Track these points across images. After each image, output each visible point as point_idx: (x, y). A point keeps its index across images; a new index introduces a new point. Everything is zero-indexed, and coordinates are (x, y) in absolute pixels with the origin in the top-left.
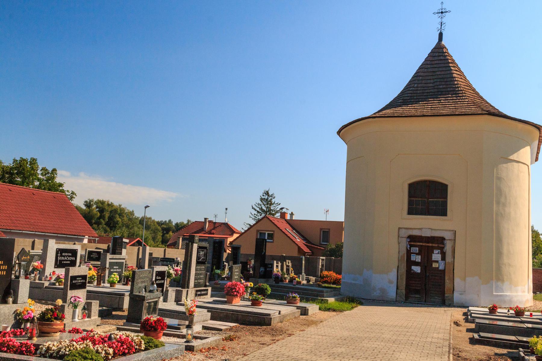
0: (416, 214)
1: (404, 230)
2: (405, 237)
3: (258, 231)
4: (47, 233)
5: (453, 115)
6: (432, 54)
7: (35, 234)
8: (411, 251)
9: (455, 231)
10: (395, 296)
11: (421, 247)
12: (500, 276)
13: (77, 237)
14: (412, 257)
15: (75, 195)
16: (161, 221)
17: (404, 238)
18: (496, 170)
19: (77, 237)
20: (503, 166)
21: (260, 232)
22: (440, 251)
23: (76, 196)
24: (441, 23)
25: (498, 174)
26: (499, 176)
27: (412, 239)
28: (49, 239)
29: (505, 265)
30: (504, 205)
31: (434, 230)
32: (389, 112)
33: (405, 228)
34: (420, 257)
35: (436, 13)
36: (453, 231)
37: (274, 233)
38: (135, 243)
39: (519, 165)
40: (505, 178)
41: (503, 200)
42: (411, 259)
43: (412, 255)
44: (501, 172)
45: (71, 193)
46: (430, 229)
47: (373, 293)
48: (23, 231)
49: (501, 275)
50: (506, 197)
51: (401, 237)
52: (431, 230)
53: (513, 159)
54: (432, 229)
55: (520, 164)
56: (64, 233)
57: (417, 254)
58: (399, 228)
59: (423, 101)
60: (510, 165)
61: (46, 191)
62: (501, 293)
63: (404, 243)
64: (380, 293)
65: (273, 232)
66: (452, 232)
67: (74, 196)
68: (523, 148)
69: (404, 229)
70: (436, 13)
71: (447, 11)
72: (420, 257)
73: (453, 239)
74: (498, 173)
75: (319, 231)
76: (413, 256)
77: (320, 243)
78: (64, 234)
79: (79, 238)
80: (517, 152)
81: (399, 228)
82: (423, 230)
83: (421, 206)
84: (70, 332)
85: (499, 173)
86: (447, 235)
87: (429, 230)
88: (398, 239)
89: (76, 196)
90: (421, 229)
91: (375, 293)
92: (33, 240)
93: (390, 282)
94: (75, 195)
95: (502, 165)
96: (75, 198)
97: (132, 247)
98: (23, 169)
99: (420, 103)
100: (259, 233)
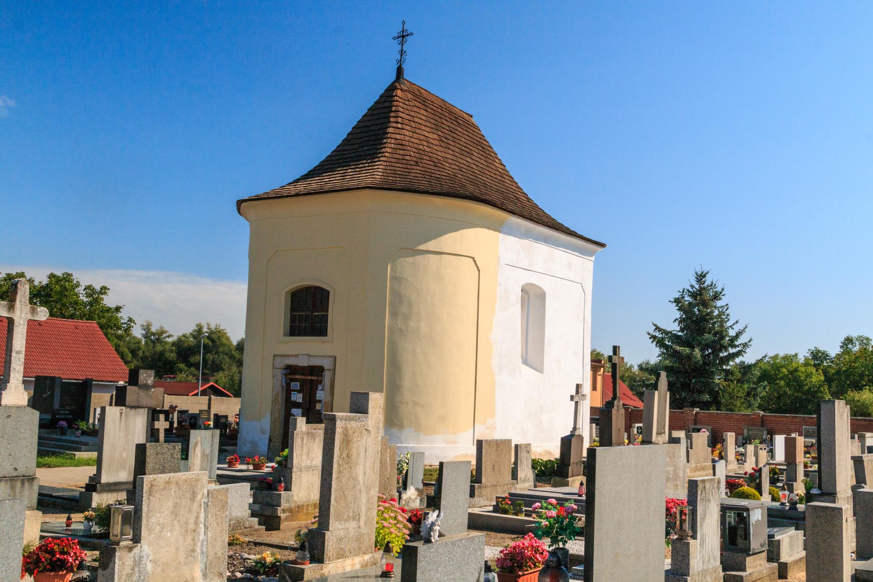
0: (299, 335)
1: (279, 359)
2: (280, 368)
4: (101, 381)
5: (322, 193)
8: (291, 388)
9: (336, 357)
10: (267, 451)
11: (303, 383)
12: (396, 420)
13: (97, 383)
14: (292, 395)
15: (134, 322)
16: (785, 358)
17: (279, 370)
18: (392, 268)
19: (97, 383)
20: (406, 260)
22: (299, 383)
23: (136, 324)
24: (402, 52)
25: (396, 272)
27: (291, 371)
28: (383, 394)
29: (407, 403)
30: (407, 317)
31: (313, 356)
33: (280, 355)
34: (301, 395)
35: (409, 35)
36: (333, 356)
38: (206, 388)
39: (442, 258)
40: (409, 279)
41: (404, 309)
42: (291, 398)
43: (292, 392)
44: (402, 270)
45: (128, 321)
46: (306, 355)
47: (243, 448)
49: (397, 419)
50: (410, 306)
51: (276, 368)
52: (307, 356)
53: (426, 249)
55: (444, 256)
56: (109, 379)
57: (299, 392)
58: (275, 356)
59: (328, 172)
60: (420, 258)
61: (59, 319)
62: (408, 444)
63: (279, 374)
64: (250, 448)
66: (332, 359)
67: (132, 324)
68: (462, 229)
69: (279, 357)
70: (409, 35)
71: (409, 33)
72: (301, 395)
73: (332, 368)
74: (396, 270)
76: (293, 394)
79: (100, 384)
80: (436, 238)
81: (275, 356)
83: (303, 323)
86: (326, 364)
87: (307, 356)
88: (273, 370)
89: (136, 324)
90: (297, 356)
91: (245, 448)
93: (263, 432)
94: (134, 322)
95: (403, 259)
96: (133, 327)
97: (195, 397)
98: (51, 290)
99: (324, 175)
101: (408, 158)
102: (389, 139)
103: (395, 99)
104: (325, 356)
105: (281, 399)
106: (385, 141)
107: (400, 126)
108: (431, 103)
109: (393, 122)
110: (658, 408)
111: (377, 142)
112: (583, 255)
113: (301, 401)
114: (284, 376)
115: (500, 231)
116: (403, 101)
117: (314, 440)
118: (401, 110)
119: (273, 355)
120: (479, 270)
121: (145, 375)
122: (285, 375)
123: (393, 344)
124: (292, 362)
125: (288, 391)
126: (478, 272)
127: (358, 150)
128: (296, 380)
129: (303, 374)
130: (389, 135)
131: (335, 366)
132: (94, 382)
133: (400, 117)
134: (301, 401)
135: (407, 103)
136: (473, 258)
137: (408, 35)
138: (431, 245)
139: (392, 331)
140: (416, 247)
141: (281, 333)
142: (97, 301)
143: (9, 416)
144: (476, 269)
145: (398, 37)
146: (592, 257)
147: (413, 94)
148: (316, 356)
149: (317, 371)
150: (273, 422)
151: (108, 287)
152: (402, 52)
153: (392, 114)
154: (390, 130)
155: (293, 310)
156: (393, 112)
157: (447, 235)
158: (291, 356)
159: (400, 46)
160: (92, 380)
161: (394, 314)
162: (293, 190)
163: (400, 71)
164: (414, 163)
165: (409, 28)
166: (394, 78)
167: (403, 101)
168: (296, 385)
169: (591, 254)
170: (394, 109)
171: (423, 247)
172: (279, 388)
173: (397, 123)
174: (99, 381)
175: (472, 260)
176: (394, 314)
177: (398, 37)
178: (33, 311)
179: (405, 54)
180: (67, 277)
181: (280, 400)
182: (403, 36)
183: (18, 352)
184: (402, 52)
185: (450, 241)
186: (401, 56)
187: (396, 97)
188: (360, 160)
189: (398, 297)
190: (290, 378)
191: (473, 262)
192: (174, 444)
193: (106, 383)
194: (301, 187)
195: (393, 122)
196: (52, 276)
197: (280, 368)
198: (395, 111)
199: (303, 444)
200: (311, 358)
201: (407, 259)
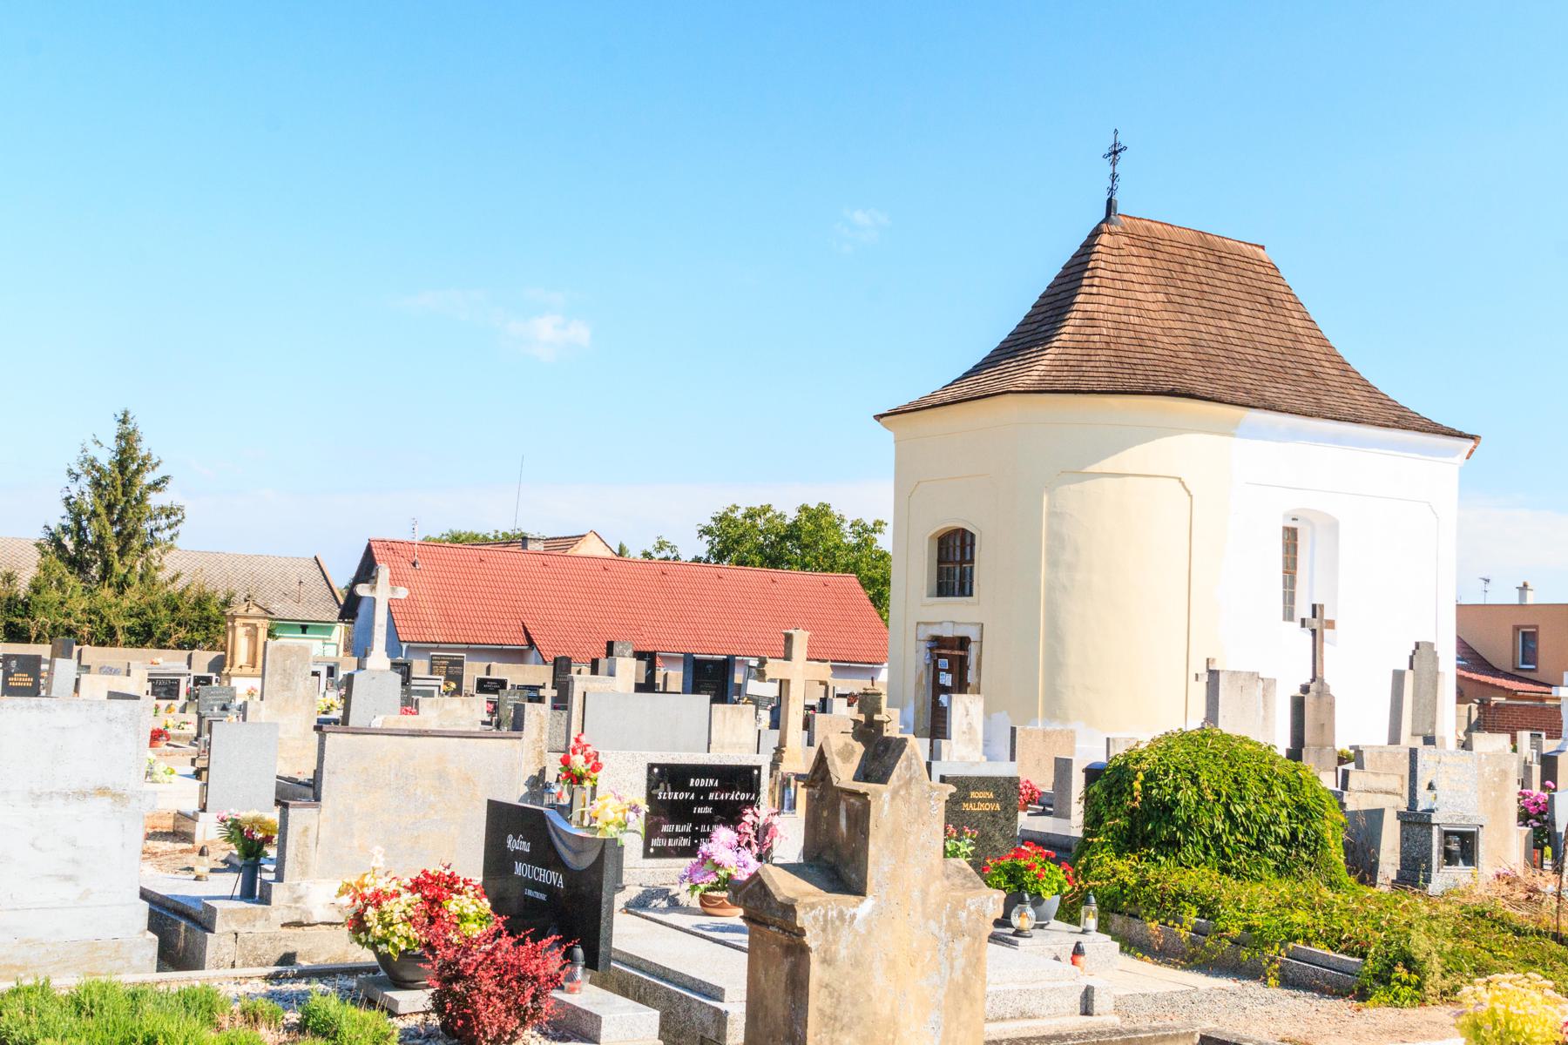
1: (922, 627)
3: (1518, 630)
4: (855, 662)
6: (1083, 250)
7: (502, 649)
9: (982, 625)
11: (951, 658)
19: (848, 665)
21: (1525, 630)
25: (1055, 506)
26: (1059, 511)
27: (938, 643)
32: (986, 381)
37: (1538, 631)
48: (744, 656)
54: (954, 622)
57: (948, 671)
58: (918, 623)
60: (1090, 485)
63: (923, 646)
65: (1534, 630)
73: (979, 639)
75: (1533, 623)
77: (1513, 665)
78: (845, 662)
79: (506, 649)
82: (944, 624)
84: (190, 668)
85: (1057, 505)
86: (972, 634)
92: (487, 664)
100: (1520, 634)
101: (1096, 338)
102: (1075, 313)
103: (1096, 250)
104: (971, 624)
105: (926, 681)
106: (1068, 316)
107: (1094, 290)
108: (1168, 243)
109: (1086, 286)
110: (1415, 703)
111: (1059, 318)
112: (1432, 456)
113: (950, 684)
114: (928, 651)
115: (1233, 435)
116: (1108, 251)
117: (742, 715)
118: (1102, 265)
119: (1537, 624)
120: (1191, 496)
121: (621, 647)
122: (931, 649)
123: (1051, 603)
124: (937, 631)
125: (937, 672)
126: (1189, 498)
127: (1036, 331)
128: (944, 656)
129: (952, 648)
130: (1075, 307)
131: (982, 637)
132: (737, 658)
133: (1098, 277)
134: (950, 684)
135: (1115, 252)
136: (1180, 479)
137: (1120, 150)
138: (1107, 465)
139: (1051, 588)
140: (1083, 468)
141: (925, 593)
142: (867, 543)
143: (373, 678)
144: (1186, 494)
145: (1110, 155)
146: (1454, 456)
147: (1126, 234)
148: (961, 623)
149: (963, 642)
150: (917, 712)
151: (885, 522)
152: (1114, 177)
153: (1087, 274)
154: (1079, 298)
155: (940, 561)
156: (1088, 269)
157: (1132, 449)
158: (935, 623)
159: (1112, 167)
160: (734, 656)
161: (1054, 564)
162: (947, 397)
163: (1110, 205)
164: (1104, 346)
165: (1123, 140)
166: (1103, 216)
167: (1108, 251)
168: (943, 663)
169: (1453, 453)
170: (1091, 265)
171: (1090, 469)
172: (922, 667)
173: (1092, 286)
174: (851, 662)
175: (1178, 481)
176: (1054, 564)
177: (1110, 155)
178: (393, 590)
179: (1117, 179)
180: (824, 510)
181: (924, 682)
182: (1115, 153)
183: (381, 626)
184: (1114, 177)
185: (1132, 458)
186: (1113, 182)
187: (1098, 247)
188: (1029, 348)
189: (1057, 538)
190: (938, 654)
191: (1180, 485)
192: (561, 711)
193: (865, 666)
194: (957, 392)
195: (1086, 286)
196: (804, 509)
197: (924, 641)
198: (1092, 269)
199: (725, 718)
200: (957, 626)
201: (1072, 487)
